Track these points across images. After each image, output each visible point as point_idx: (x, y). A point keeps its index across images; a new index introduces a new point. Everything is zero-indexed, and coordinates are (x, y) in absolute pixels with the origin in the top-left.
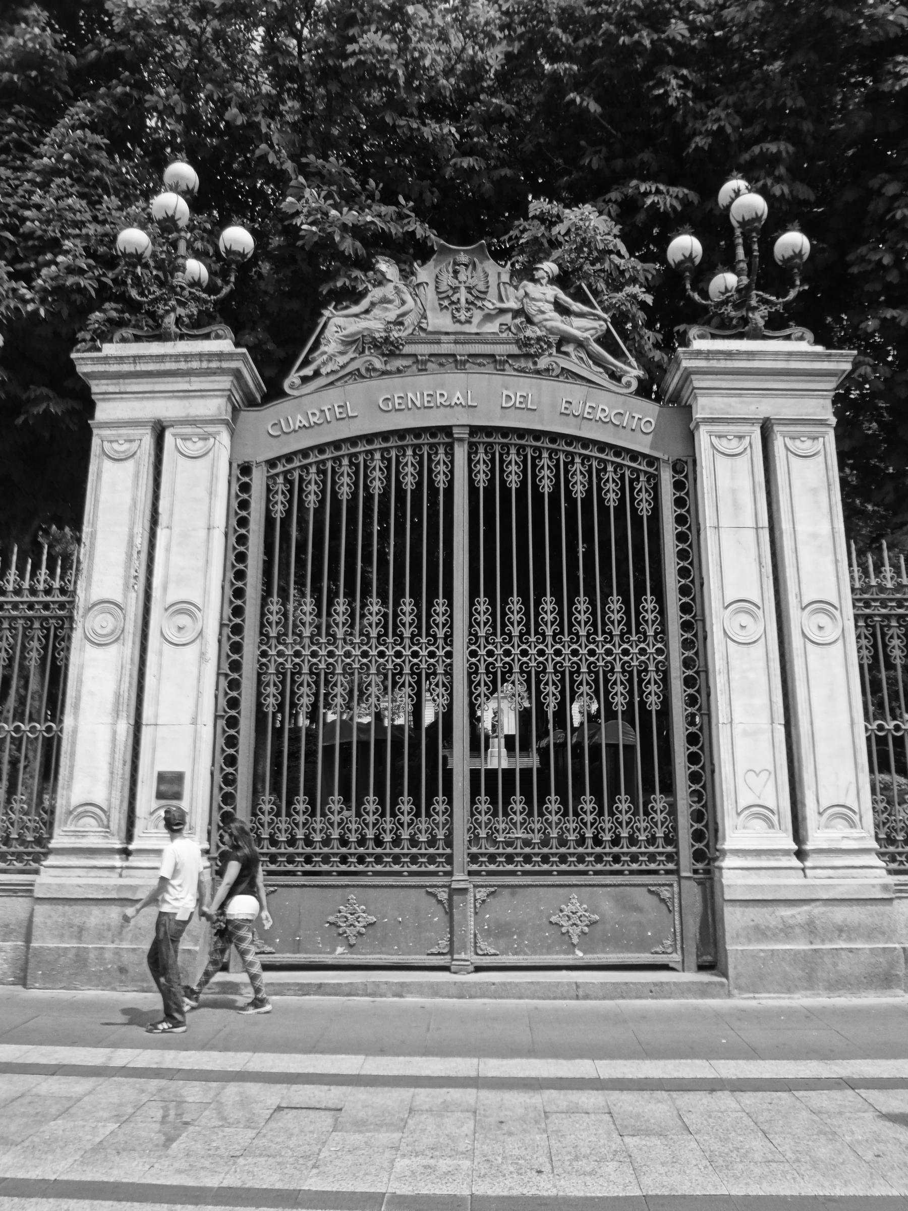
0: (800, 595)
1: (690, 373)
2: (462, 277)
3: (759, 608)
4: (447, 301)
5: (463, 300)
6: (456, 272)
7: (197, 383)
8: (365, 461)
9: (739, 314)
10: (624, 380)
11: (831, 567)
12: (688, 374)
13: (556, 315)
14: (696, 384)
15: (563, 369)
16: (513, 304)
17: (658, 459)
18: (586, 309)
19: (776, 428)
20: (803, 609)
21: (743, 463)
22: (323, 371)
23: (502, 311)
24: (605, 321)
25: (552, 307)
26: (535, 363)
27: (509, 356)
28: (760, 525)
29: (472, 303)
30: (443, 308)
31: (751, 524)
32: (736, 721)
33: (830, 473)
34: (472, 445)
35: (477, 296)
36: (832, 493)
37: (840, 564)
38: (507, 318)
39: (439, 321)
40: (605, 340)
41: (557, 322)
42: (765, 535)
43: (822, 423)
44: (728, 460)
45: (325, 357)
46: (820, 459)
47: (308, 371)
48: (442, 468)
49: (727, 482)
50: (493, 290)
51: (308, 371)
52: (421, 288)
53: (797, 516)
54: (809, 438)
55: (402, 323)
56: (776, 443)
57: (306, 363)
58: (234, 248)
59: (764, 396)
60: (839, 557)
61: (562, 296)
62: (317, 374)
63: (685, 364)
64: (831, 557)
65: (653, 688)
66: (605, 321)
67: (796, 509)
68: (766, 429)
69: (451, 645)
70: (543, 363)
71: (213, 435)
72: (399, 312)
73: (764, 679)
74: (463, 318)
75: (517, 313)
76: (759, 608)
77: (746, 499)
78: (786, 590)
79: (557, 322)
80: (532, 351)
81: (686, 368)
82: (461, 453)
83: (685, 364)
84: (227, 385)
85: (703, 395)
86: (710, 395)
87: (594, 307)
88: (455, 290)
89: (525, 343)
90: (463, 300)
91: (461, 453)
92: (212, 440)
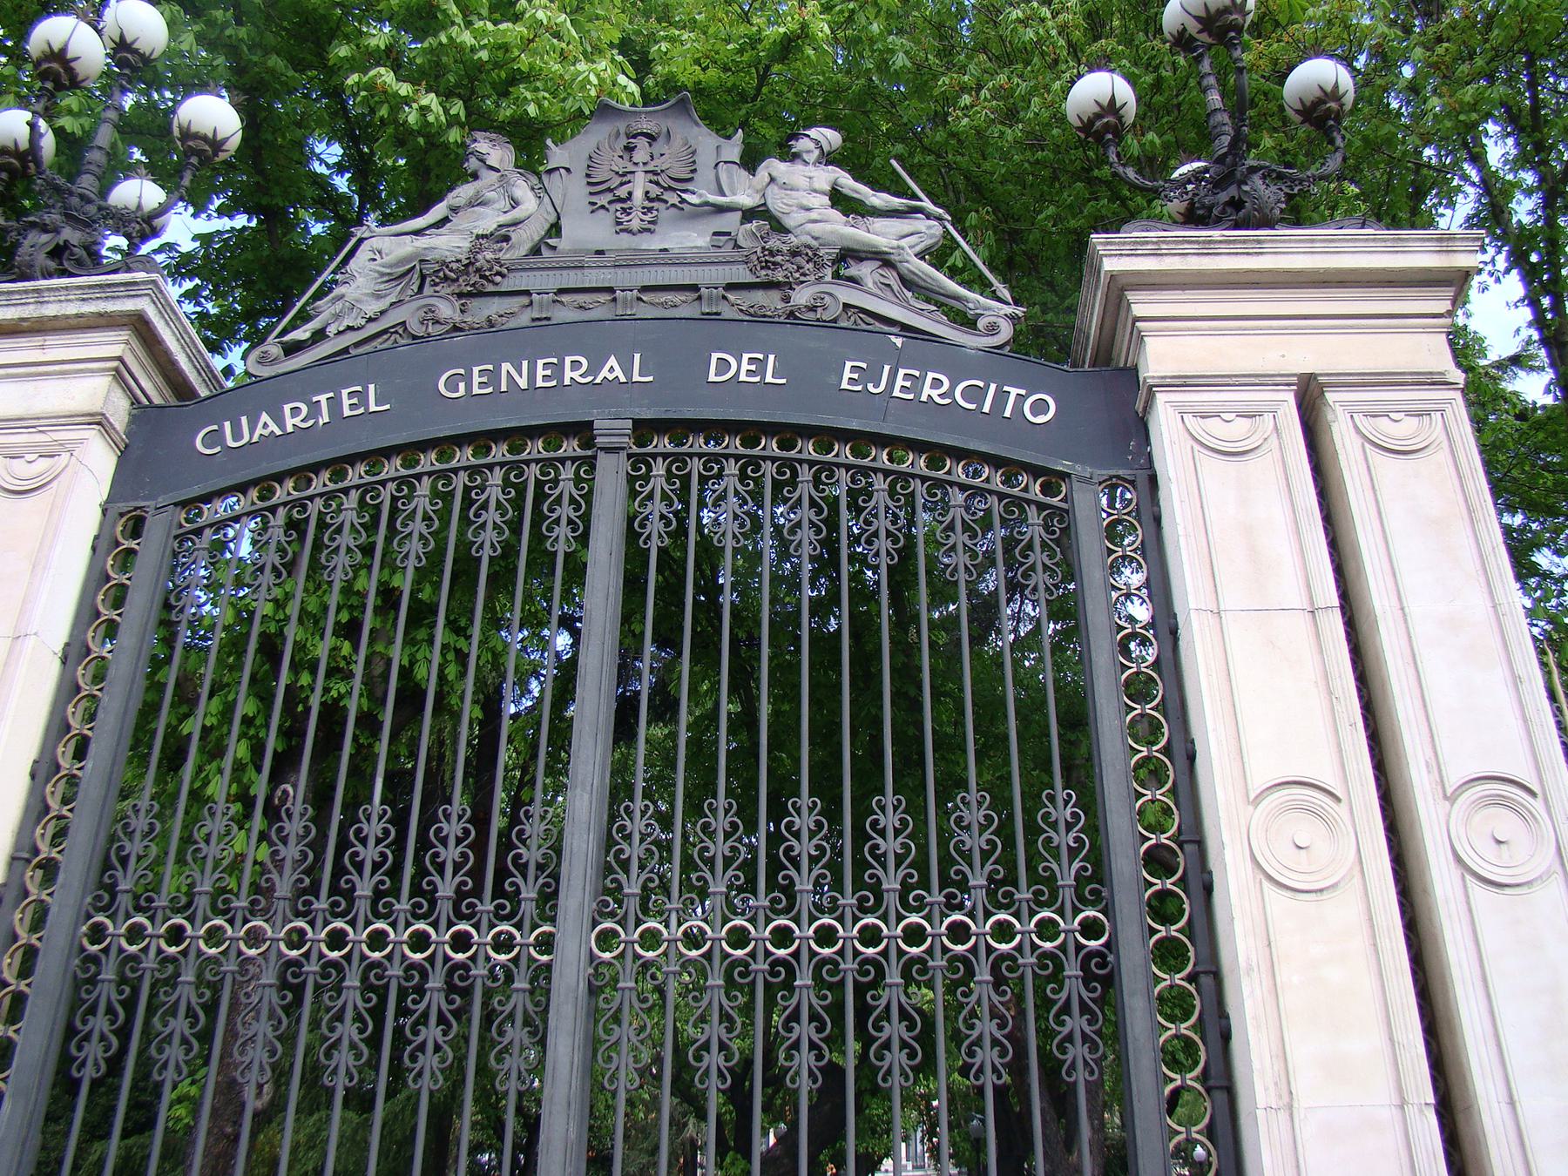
0: (1436, 764)
1: (1123, 289)
2: (640, 155)
3: (1338, 800)
4: (607, 194)
5: (638, 195)
6: (629, 149)
7: (59, 348)
8: (394, 499)
9: (1223, 197)
10: (981, 324)
11: (1505, 696)
12: (1120, 287)
13: (836, 214)
14: (1137, 310)
15: (846, 306)
16: (747, 200)
17: (1064, 476)
18: (897, 202)
19: (1330, 396)
20: (1451, 799)
21: (1262, 468)
22: (332, 330)
23: (721, 209)
24: (939, 219)
25: (826, 200)
26: (787, 299)
27: (731, 287)
28: (1320, 603)
29: (658, 199)
30: (595, 208)
31: (1297, 599)
32: (1302, 1101)
33: (1470, 486)
34: (637, 460)
35: (670, 189)
36: (1481, 526)
37: (1525, 688)
38: (731, 222)
39: (587, 230)
40: (939, 255)
41: (839, 228)
42: (1334, 625)
43: (1435, 381)
44: (1230, 466)
45: (339, 306)
46: (1443, 456)
47: (302, 334)
48: (566, 511)
49: (1229, 531)
50: (705, 174)
51: (302, 334)
52: (556, 175)
53: (1406, 581)
54: (1409, 414)
55: (506, 239)
56: (1335, 428)
57: (304, 317)
58: (194, 129)
59: (1298, 331)
60: (1521, 671)
61: (847, 182)
62: (320, 335)
63: (1109, 265)
64: (1500, 673)
65: (1075, 1023)
66: (939, 219)
67: (1402, 566)
68: (1310, 397)
69: (552, 920)
70: (801, 296)
71: (69, 448)
72: (503, 219)
73: (1368, 984)
74: (636, 225)
75: (749, 215)
76: (1338, 800)
77: (1280, 547)
78: (1401, 755)
79: (839, 228)
80: (779, 276)
81: (1113, 276)
82: (611, 475)
83: (1109, 265)
84: (117, 350)
85: (1159, 333)
86: (1176, 333)
87: (914, 197)
88: (625, 177)
89: (768, 261)
90: (638, 195)
91: (611, 475)
92: (65, 457)
